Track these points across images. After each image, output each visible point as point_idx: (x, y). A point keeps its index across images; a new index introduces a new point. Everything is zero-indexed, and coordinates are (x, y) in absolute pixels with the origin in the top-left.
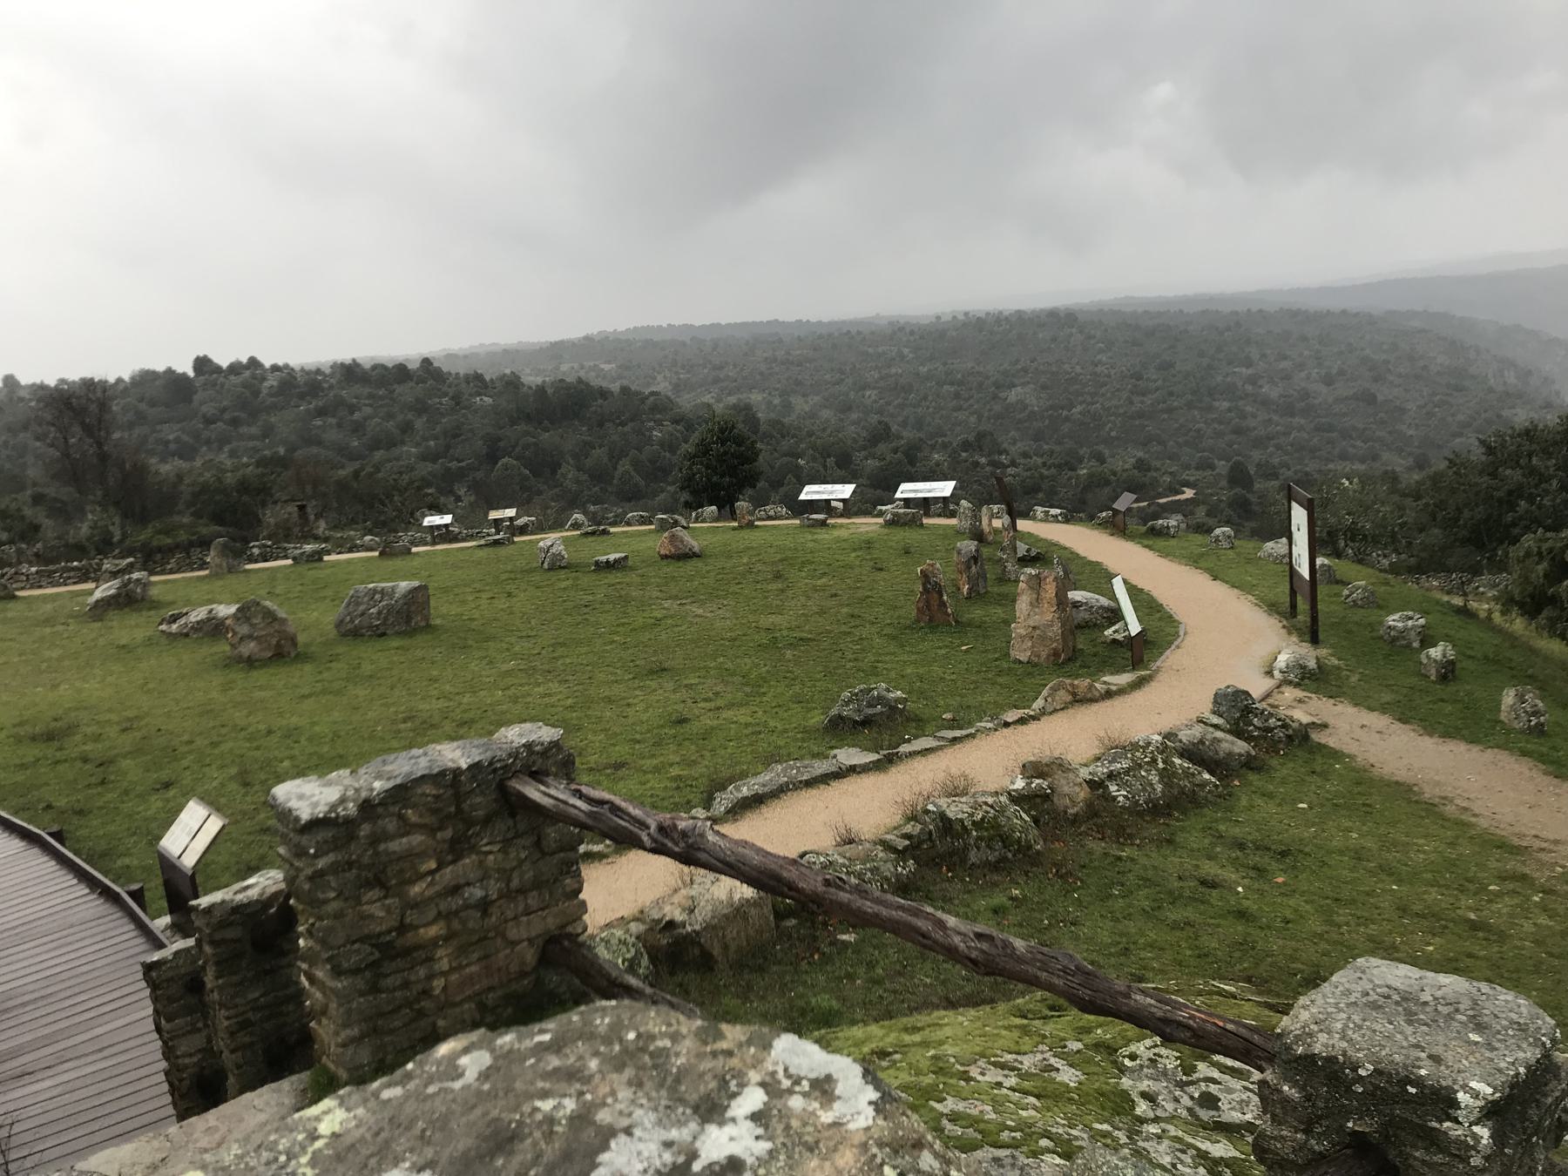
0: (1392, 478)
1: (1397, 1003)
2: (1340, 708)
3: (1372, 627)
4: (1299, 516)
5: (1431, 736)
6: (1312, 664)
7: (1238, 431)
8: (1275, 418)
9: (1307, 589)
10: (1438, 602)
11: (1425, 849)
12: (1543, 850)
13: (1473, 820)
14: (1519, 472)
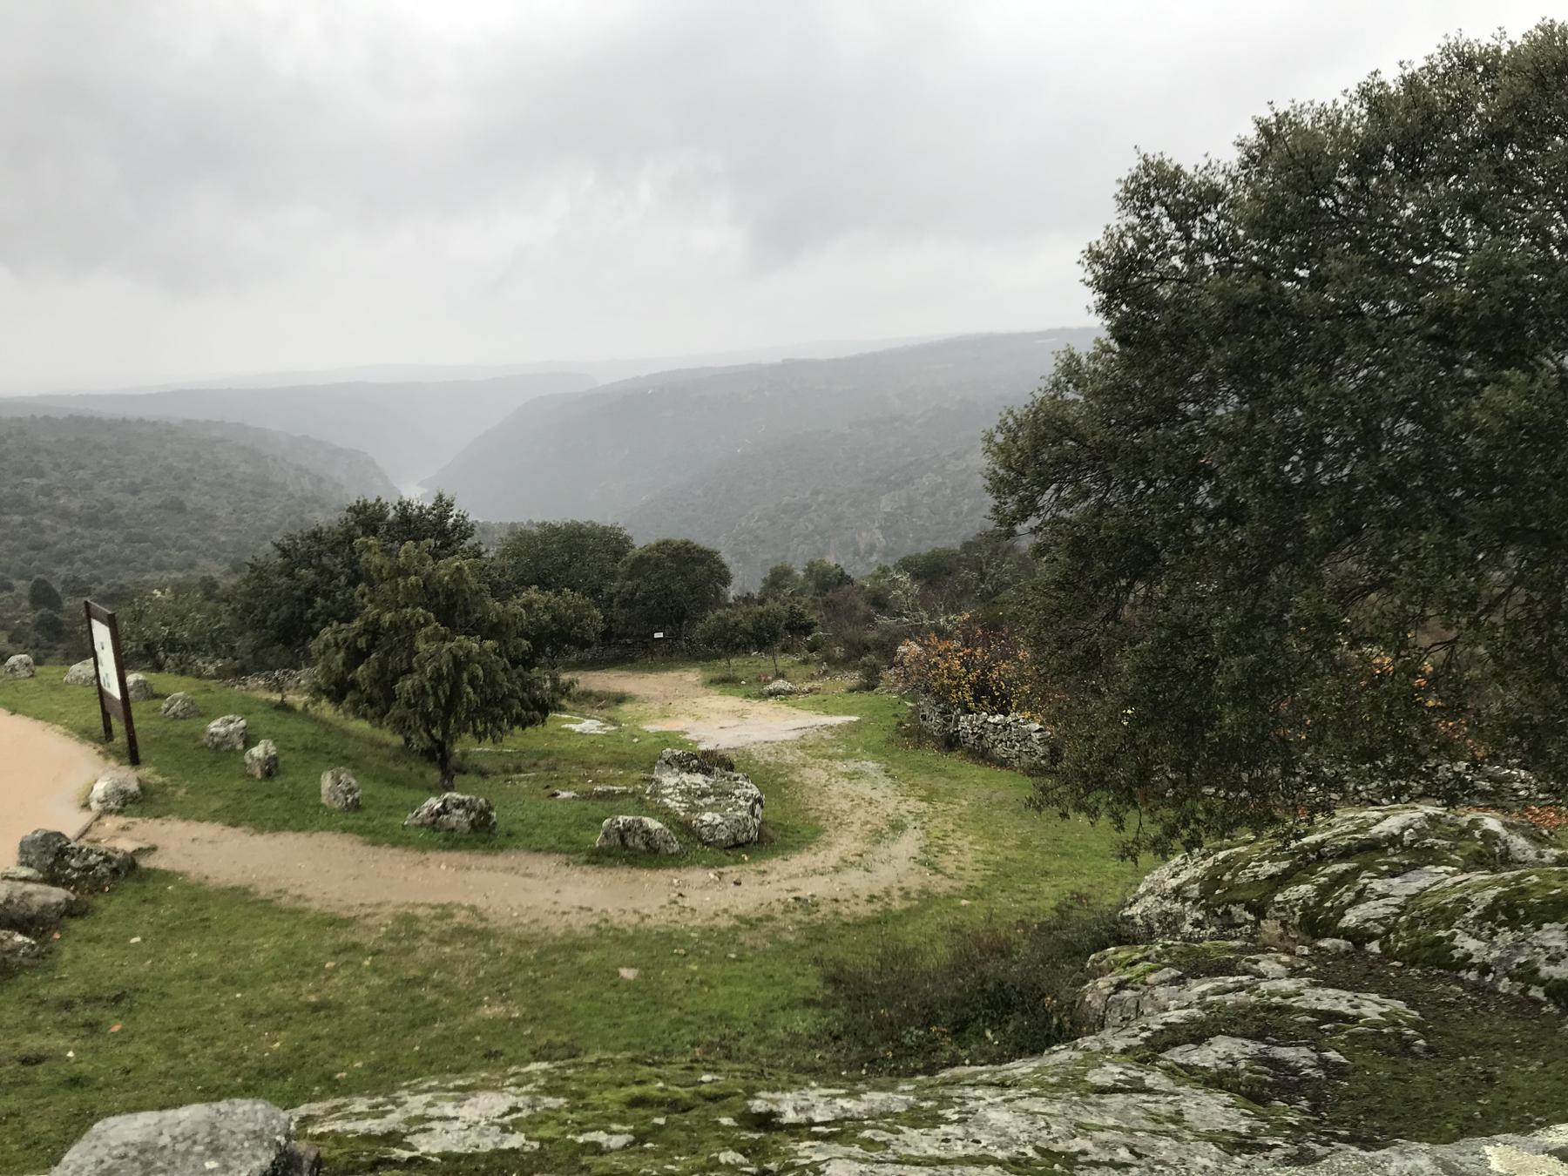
0: (209, 587)
1: (135, 1159)
2: (168, 826)
3: (195, 737)
4: (101, 634)
5: (261, 832)
6: (133, 787)
7: (36, 548)
8: (79, 530)
9: (120, 708)
10: (258, 702)
11: (265, 948)
12: (367, 916)
13: (306, 905)
14: (312, 571)
